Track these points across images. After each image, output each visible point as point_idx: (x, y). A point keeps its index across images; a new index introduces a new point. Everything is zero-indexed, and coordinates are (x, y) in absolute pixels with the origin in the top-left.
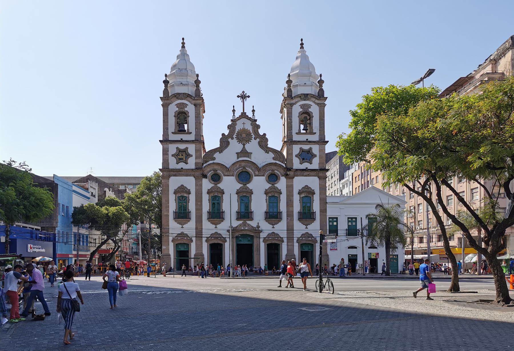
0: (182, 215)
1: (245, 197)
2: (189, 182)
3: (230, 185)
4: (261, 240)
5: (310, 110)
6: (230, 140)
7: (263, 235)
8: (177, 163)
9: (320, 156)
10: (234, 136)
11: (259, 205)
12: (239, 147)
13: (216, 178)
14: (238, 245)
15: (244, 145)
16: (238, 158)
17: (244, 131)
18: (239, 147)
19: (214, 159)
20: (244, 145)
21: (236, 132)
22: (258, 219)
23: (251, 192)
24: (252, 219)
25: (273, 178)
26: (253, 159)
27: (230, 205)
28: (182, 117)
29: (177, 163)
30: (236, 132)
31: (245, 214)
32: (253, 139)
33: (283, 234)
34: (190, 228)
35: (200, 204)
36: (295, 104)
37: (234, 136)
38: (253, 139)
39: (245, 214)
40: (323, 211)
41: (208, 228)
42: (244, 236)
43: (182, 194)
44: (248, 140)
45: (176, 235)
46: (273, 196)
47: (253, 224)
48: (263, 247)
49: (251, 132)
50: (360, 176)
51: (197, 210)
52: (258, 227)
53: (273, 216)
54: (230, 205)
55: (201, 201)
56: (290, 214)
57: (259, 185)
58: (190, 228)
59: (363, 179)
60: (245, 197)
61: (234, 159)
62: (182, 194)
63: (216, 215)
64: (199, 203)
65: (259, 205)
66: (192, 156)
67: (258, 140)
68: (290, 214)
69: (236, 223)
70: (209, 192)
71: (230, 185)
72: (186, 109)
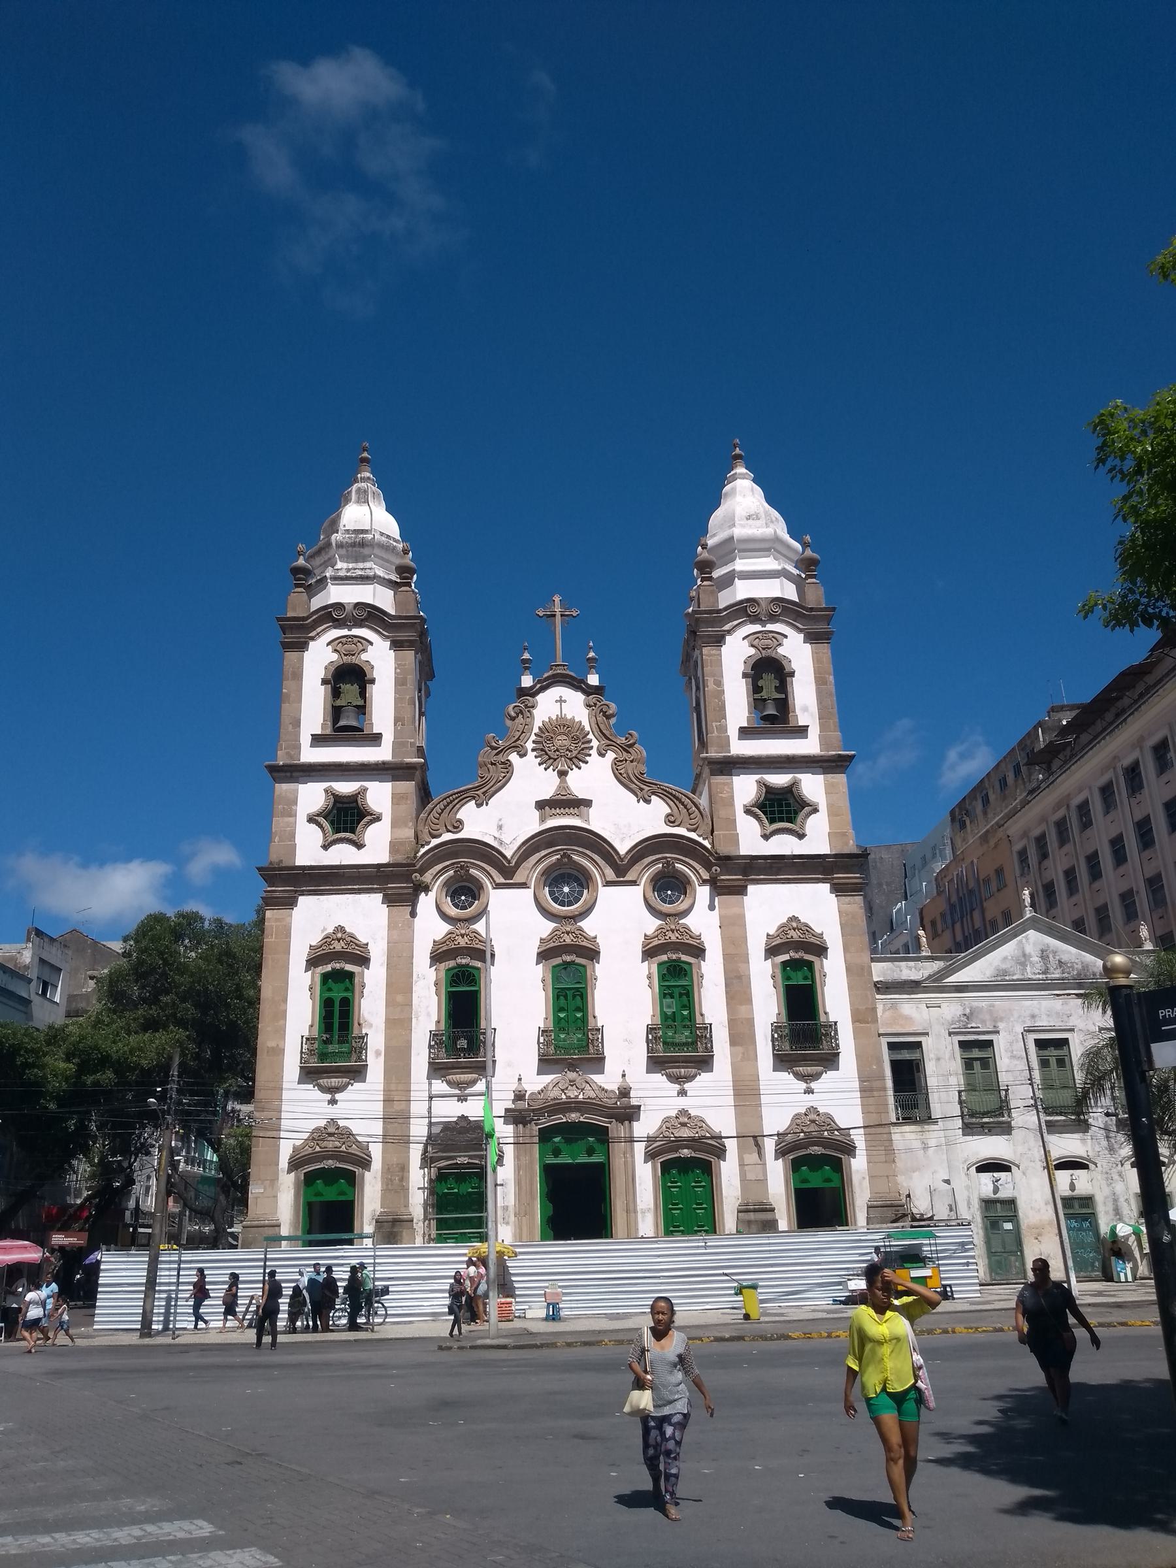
0: (336, 1049)
1: (569, 968)
2: (364, 916)
3: (514, 922)
4: (640, 1149)
5: (780, 650)
6: (514, 757)
7: (646, 1126)
8: (325, 847)
9: (830, 807)
10: (530, 745)
11: (624, 1002)
12: (546, 783)
13: (465, 891)
14: (550, 1172)
15: (562, 774)
16: (543, 820)
17: (562, 726)
18: (546, 783)
19: (458, 826)
20: (562, 774)
21: (536, 730)
22: (625, 1058)
23: (593, 954)
24: (598, 1063)
25: (670, 885)
26: (597, 822)
27: (517, 1005)
28: (350, 690)
29: (325, 847)
30: (536, 730)
31: (571, 1034)
32: (594, 752)
33: (721, 1119)
34: (360, 1109)
35: (401, 1006)
36: (729, 632)
37: (530, 745)
38: (594, 752)
39: (571, 1034)
40: (863, 1017)
41: (435, 1104)
42: (572, 1132)
43: (338, 966)
44: (578, 758)
45: (306, 1136)
46: (674, 963)
47: (608, 1080)
48: (645, 1175)
49: (588, 728)
50: (949, 917)
51: (391, 1023)
52: (625, 1093)
53: (679, 1044)
54: (517, 1005)
55: (408, 990)
56: (741, 1034)
57: (619, 918)
58: (360, 1109)
59: (958, 926)
60: (569, 968)
61: (531, 824)
62: (338, 966)
63: (464, 1030)
64: (400, 998)
65: (624, 1002)
66: (378, 818)
67: (611, 756)
68: (741, 1034)
69: (536, 1083)
70: (437, 957)
71: (514, 922)
72: (364, 657)
